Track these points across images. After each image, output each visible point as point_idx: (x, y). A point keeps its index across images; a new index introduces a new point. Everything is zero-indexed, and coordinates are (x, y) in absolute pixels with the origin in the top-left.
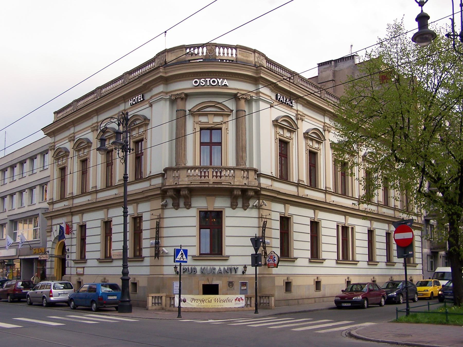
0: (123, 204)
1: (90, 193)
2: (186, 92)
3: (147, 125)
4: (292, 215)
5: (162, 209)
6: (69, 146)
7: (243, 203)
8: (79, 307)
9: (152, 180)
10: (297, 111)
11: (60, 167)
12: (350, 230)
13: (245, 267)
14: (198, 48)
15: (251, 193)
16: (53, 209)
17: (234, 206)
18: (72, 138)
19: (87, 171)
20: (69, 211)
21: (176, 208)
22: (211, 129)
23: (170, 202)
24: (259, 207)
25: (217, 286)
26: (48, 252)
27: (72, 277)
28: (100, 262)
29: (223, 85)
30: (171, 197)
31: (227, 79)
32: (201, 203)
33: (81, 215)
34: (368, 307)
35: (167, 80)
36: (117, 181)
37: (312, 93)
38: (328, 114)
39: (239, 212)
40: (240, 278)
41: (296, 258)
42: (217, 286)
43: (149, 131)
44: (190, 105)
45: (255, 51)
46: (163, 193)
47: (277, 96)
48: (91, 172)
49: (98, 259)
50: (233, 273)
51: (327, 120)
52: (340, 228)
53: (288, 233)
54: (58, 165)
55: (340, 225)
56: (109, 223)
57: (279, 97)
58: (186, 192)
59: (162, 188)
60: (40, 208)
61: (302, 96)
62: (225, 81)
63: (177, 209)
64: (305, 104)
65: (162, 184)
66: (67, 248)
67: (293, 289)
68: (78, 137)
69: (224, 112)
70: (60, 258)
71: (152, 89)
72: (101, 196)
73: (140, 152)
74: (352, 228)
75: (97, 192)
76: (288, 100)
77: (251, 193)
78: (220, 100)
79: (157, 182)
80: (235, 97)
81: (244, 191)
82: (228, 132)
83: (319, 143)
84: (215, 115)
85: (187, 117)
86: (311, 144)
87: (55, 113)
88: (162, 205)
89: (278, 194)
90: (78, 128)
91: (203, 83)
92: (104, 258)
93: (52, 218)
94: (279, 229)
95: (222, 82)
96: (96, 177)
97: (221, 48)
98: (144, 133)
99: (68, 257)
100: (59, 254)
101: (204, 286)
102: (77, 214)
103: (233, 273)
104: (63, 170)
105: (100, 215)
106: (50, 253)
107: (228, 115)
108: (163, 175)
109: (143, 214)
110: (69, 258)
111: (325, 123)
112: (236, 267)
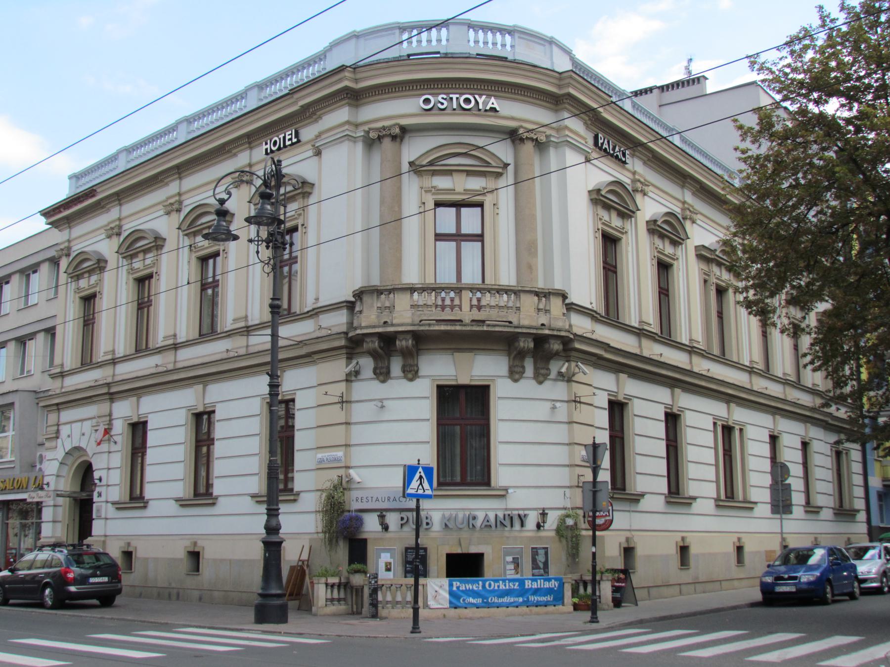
0: (268, 367)
1: (101, 365)
2: (404, 122)
3: (306, 195)
4: (630, 398)
5: (347, 380)
6: (107, 248)
7: (536, 369)
8: (11, 601)
9: (321, 317)
10: (634, 173)
11: (83, 294)
12: (737, 433)
13: (544, 514)
14: (429, 29)
15: (556, 346)
16: (62, 387)
17: (515, 374)
18: (176, 206)
19: (94, 318)
20: (105, 390)
21: (381, 378)
22: (458, 205)
23: (367, 364)
24: (567, 378)
25: (479, 557)
26: (48, 484)
27: (108, 542)
28: (117, 509)
29: (488, 108)
30: (374, 354)
31: (496, 97)
32: (440, 368)
33: (135, 399)
34: (834, 602)
35: (354, 97)
36: (102, 354)
37: (663, 137)
38: (690, 184)
39: (527, 386)
40: (531, 539)
41: (642, 495)
42: (479, 557)
43: (312, 211)
44: (414, 149)
45: (551, 42)
46: (353, 345)
47: (596, 138)
48: (104, 321)
49: (177, 500)
50: (517, 526)
51: (689, 197)
52: (719, 430)
53: (622, 439)
54: (132, 271)
55: (719, 423)
56: (141, 426)
57: (600, 141)
58: (410, 342)
59: (350, 335)
60: (16, 391)
61: (645, 141)
62: (493, 100)
63: (383, 382)
64: (649, 160)
65: (350, 324)
66: (96, 475)
67: (692, 561)
68: (129, 227)
69: (491, 170)
70: (75, 499)
71: (320, 117)
72: (187, 356)
73: (146, 299)
74: (741, 430)
75: (114, 362)
76: (617, 149)
77: (556, 346)
78: (480, 141)
79: (338, 321)
80: (513, 136)
81: (540, 340)
82: (497, 211)
83: (675, 243)
84: (469, 173)
85: (405, 177)
86: (661, 247)
87: (70, 178)
88: (348, 375)
89: (606, 351)
90: (129, 208)
91: (442, 104)
92: (127, 499)
93: (59, 407)
94: (607, 427)
95: (485, 103)
96: (175, 313)
97: (480, 31)
98: (300, 215)
99: (100, 495)
100: (74, 489)
101: (450, 557)
102: (121, 398)
103: (517, 526)
104: (89, 300)
105: (187, 399)
106: (52, 487)
107: (499, 175)
108: (350, 306)
109: (298, 393)
110: (103, 498)
111: (684, 203)
112: (521, 512)
